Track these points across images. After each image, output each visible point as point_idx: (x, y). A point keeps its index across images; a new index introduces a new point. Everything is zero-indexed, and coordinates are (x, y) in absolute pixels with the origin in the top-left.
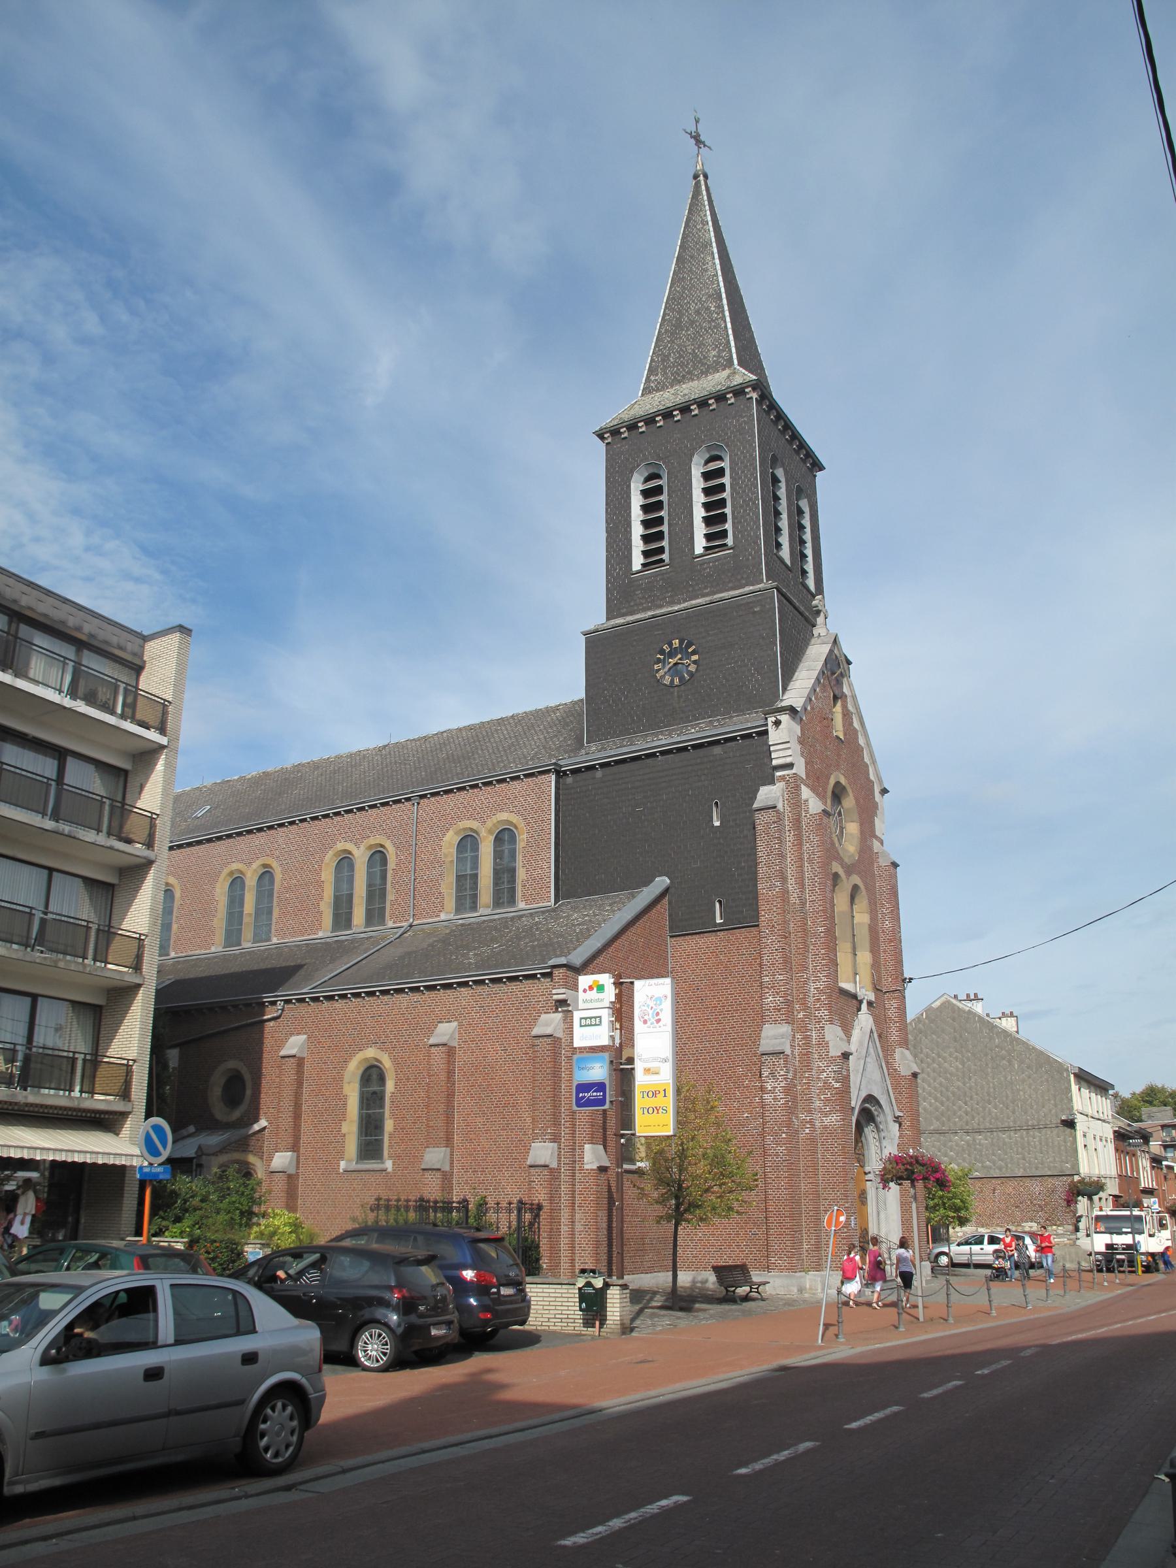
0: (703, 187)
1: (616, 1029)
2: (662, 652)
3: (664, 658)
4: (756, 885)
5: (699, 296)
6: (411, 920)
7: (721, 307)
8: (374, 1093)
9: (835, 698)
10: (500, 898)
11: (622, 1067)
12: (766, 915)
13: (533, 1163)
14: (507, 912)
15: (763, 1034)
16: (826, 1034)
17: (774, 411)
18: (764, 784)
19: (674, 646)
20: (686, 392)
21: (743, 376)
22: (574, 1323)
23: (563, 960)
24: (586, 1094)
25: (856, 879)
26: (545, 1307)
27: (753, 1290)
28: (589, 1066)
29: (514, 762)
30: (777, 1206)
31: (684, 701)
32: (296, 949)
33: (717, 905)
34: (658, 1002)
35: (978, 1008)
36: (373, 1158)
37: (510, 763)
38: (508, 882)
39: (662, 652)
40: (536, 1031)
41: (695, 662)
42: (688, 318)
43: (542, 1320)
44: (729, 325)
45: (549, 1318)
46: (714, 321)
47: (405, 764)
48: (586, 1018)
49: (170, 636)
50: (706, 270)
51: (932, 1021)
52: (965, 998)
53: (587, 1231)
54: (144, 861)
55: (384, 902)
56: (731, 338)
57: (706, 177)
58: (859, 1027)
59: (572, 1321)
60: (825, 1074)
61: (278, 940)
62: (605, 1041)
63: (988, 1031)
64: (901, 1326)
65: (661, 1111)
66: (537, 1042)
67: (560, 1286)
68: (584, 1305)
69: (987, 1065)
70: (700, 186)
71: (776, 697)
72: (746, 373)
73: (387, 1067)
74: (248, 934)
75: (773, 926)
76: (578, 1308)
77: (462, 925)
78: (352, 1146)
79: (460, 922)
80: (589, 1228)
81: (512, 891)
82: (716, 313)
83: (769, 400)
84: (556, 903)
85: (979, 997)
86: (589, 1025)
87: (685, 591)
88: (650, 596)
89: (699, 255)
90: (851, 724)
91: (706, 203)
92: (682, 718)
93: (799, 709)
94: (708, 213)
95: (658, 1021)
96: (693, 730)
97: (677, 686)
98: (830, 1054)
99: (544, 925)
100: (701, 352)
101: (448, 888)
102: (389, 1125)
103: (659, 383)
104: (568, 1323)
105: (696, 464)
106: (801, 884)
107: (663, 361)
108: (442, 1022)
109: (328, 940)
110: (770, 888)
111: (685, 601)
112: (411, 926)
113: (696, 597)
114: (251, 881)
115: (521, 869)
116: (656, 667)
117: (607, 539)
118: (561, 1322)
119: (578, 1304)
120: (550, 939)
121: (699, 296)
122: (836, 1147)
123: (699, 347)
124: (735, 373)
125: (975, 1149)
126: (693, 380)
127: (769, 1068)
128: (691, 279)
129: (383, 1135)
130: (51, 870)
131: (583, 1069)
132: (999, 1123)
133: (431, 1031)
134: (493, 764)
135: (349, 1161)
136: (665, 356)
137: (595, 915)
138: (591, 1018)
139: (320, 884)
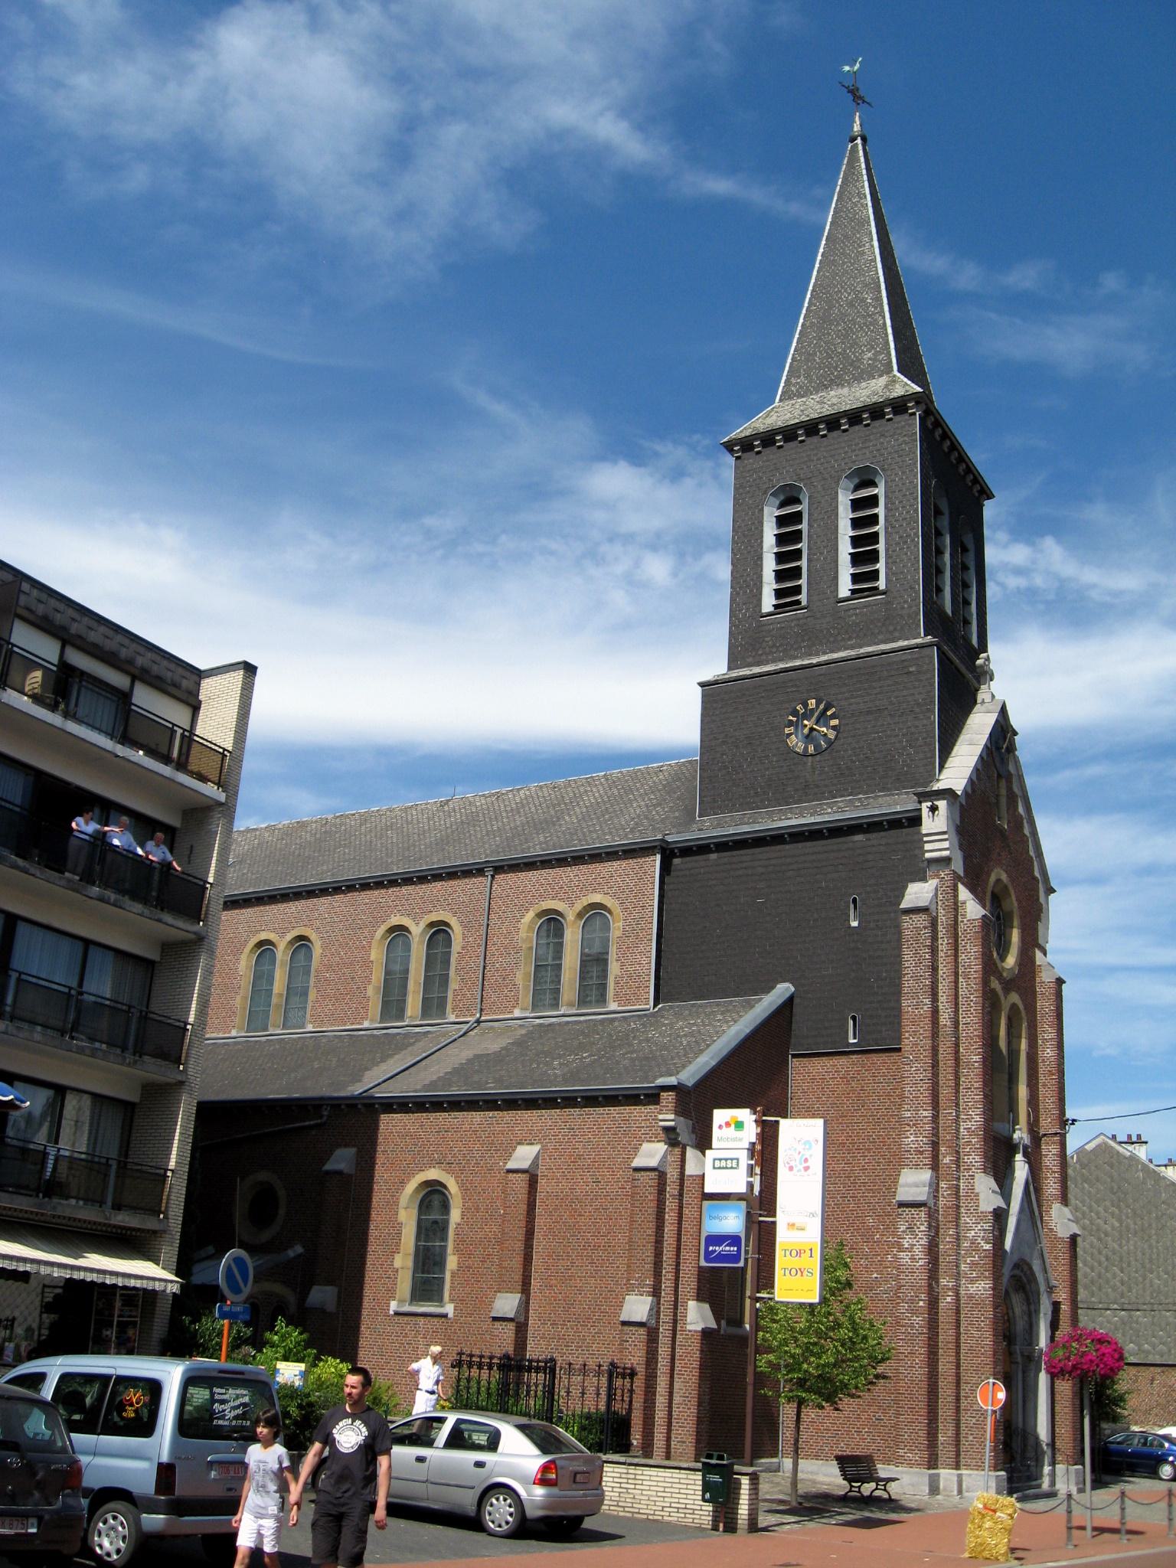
0: (861, 153)
1: (756, 1174)
2: (795, 713)
3: (797, 721)
4: (899, 1001)
5: (853, 285)
6: (478, 1015)
7: (880, 299)
8: (435, 1222)
9: (999, 776)
10: (587, 996)
11: (761, 1219)
12: (914, 1037)
13: (627, 1319)
14: (593, 1014)
15: (902, 1180)
16: (976, 1185)
17: (978, 485)
18: (913, 881)
19: (810, 707)
20: (835, 400)
21: (905, 386)
22: (693, 1514)
23: (672, 1081)
24: (717, 1248)
25: (1014, 998)
26: (659, 1494)
27: (853, 1489)
28: (722, 1214)
29: (611, 833)
30: (909, 1387)
31: (819, 774)
32: (336, 1040)
33: (851, 1022)
34: (807, 1147)
35: (1141, 1152)
36: (430, 1300)
37: (605, 834)
38: (598, 977)
39: (795, 713)
40: (638, 1162)
41: (834, 728)
42: (839, 310)
43: (654, 1508)
45: (663, 1507)
46: (870, 316)
47: (474, 826)
48: (720, 1160)
49: (232, 674)
50: (863, 253)
51: (1083, 1166)
52: (1126, 1140)
53: (686, 1405)
54: (193, 936)
55: (446, 991)
56: (891, 338)
57: (864, 139)
59: (691, 1511)
60: (973, 1232)
61: (314, 1027)
62: (742, 1188)
63: (1153, 1182)
65: (805, 1273)
66: (638, 1175)
67: (678, 1471)
68: (708, 1495)
69: (1150, 1225)
70: (858, 152)
71: (932, 778)
72: (909, 382)
73: (452, 1192)
74: (275, 1017)
76: (700, 1498)
77: (541, 1025)
78: (404, 1284)
79: (538, 1021)
80: (689, 1401)
81: (603, 987)
82: (873, 306)
84: (655, 1006)
85: (1143, 1140)
86: (723, 1168)
87: (824, 641)
88: (781, 645)
89: (854, 234)
90: (1016, 808)
91: (864, 172)
92: (816, 794)
93: (959, 793)
94: (866, 184)
95: (807, 1169)
96: (830, 810)
97: (811, 755)
98: (981, 1209)
99: (643, 1032)
100: (853, 353)
101: (523, 977)
102: (452, 1262)
103: (801, 387)
104: (685, 1513)
105: (844, 489)
107: (807, 360)
108: (523, 1144)
109: (375, 1032)
110: (917, 1006)
111: (825, 653)
112: (478, 1022)
113: (839, 650)
114: (282, 953)
115: (615, 963)
116: (787, 731)
117: (732, 573)
118: (678, 1512)
119: (701, 1493)
120: (651, 1051)
121: (853, 285)
122: (982, 1321)
123: (852, 346)
124: (894, 381)
125: (1131, 1328)
126: (843, 386)
128: (844, 263)
129: (444, 1273)
130: (87, 943)
131: (714, 1218)
132: (1162, 1298)
133: (508, 1155)
134: (584, 834)
135: (401, 1301)
136: (809, 354)
137: (704, 1025)
138: (726, 1160)
139: (367, 964)
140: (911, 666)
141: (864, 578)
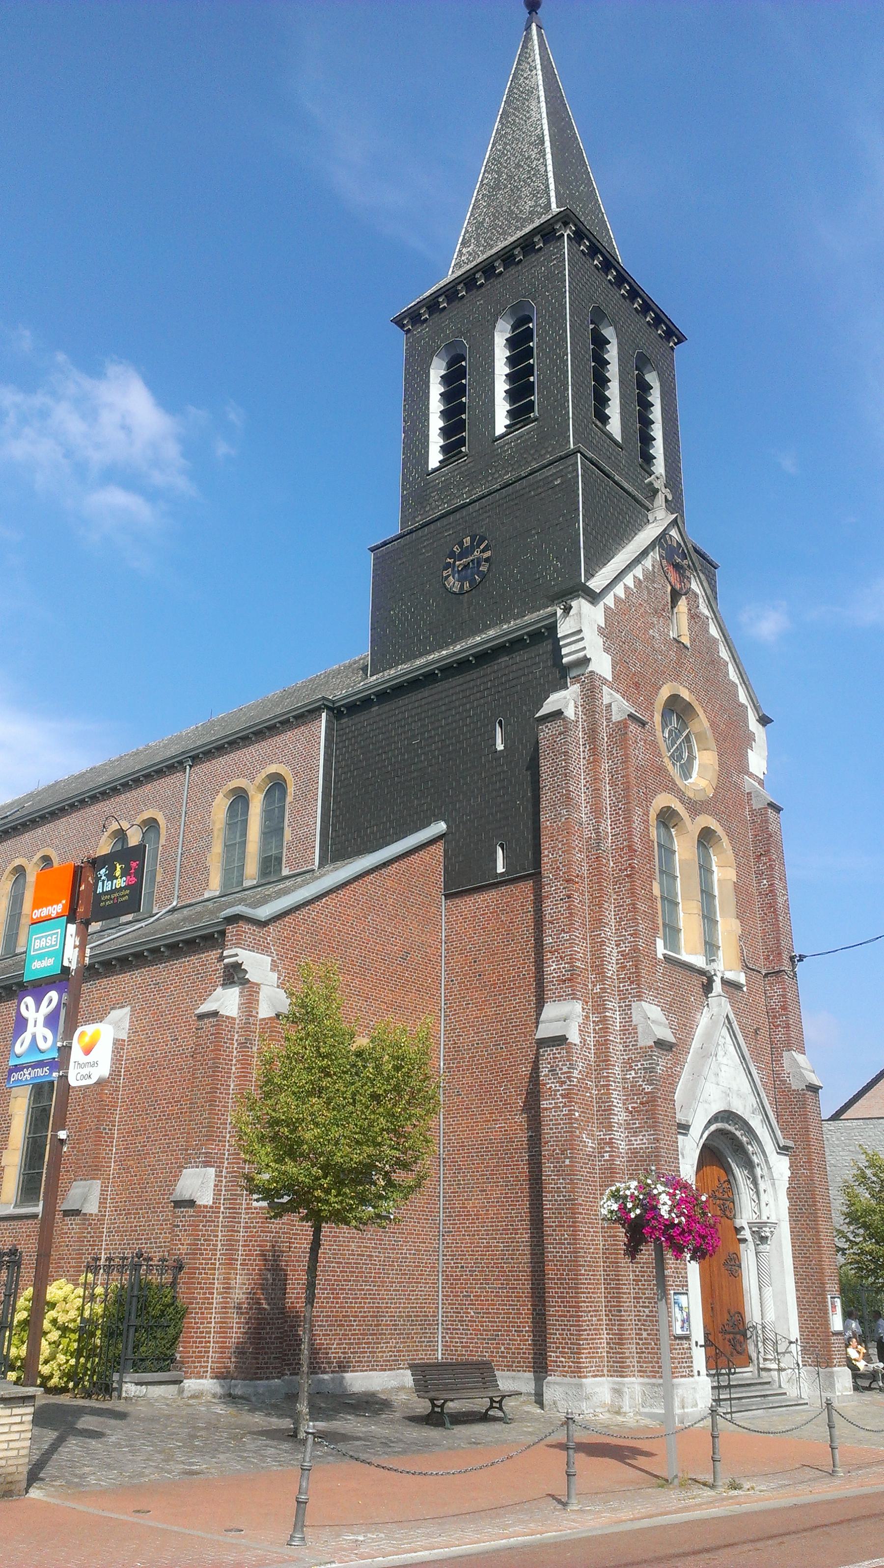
2: (452, 555)
7: (542, 153)
16: (634, 1016)
39: (452, 555)
44: (550, 168)
56: (551, 181)
58: (709, 1015)
60: (633, 1072)
64: (573, 1500)
75: (558, 868)
83: (641, 297)
88: (446, 496)
106: (597, 811)
127: (549, 1063)
140: (556, 479)
141: (518, 415)
